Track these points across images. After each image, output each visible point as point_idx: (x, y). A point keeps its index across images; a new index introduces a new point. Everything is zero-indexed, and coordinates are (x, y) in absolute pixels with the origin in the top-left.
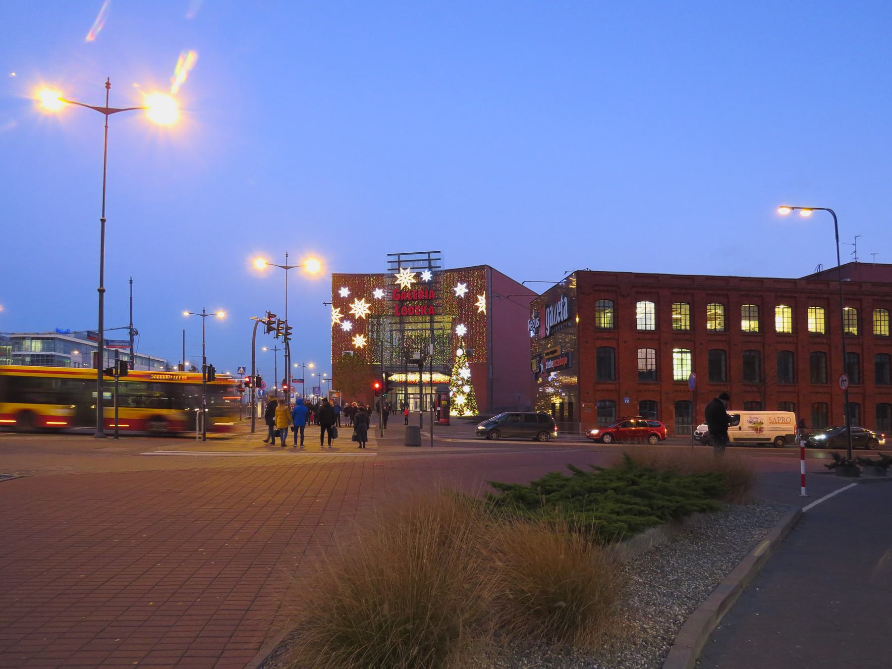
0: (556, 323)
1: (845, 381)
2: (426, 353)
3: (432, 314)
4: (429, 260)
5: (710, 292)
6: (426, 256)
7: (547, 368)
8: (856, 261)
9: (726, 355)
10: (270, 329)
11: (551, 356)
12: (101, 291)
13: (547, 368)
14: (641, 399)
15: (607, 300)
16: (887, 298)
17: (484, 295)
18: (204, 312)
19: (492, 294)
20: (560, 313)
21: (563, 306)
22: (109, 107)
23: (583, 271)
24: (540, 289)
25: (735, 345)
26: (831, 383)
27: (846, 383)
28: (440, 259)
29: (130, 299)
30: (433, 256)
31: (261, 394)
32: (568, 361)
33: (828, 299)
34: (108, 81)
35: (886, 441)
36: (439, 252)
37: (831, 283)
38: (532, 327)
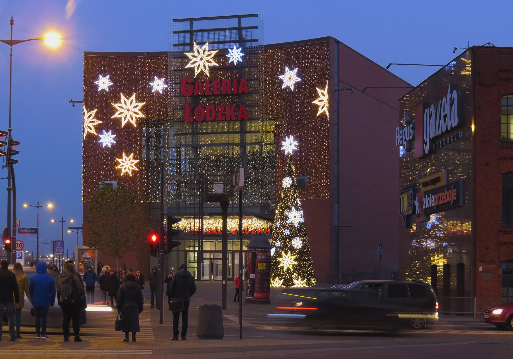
4: (240, 29)
6: (234, 23)
17: (327, 88)
30: (246, 22)
32: (458, 196)
36: (256, 15)
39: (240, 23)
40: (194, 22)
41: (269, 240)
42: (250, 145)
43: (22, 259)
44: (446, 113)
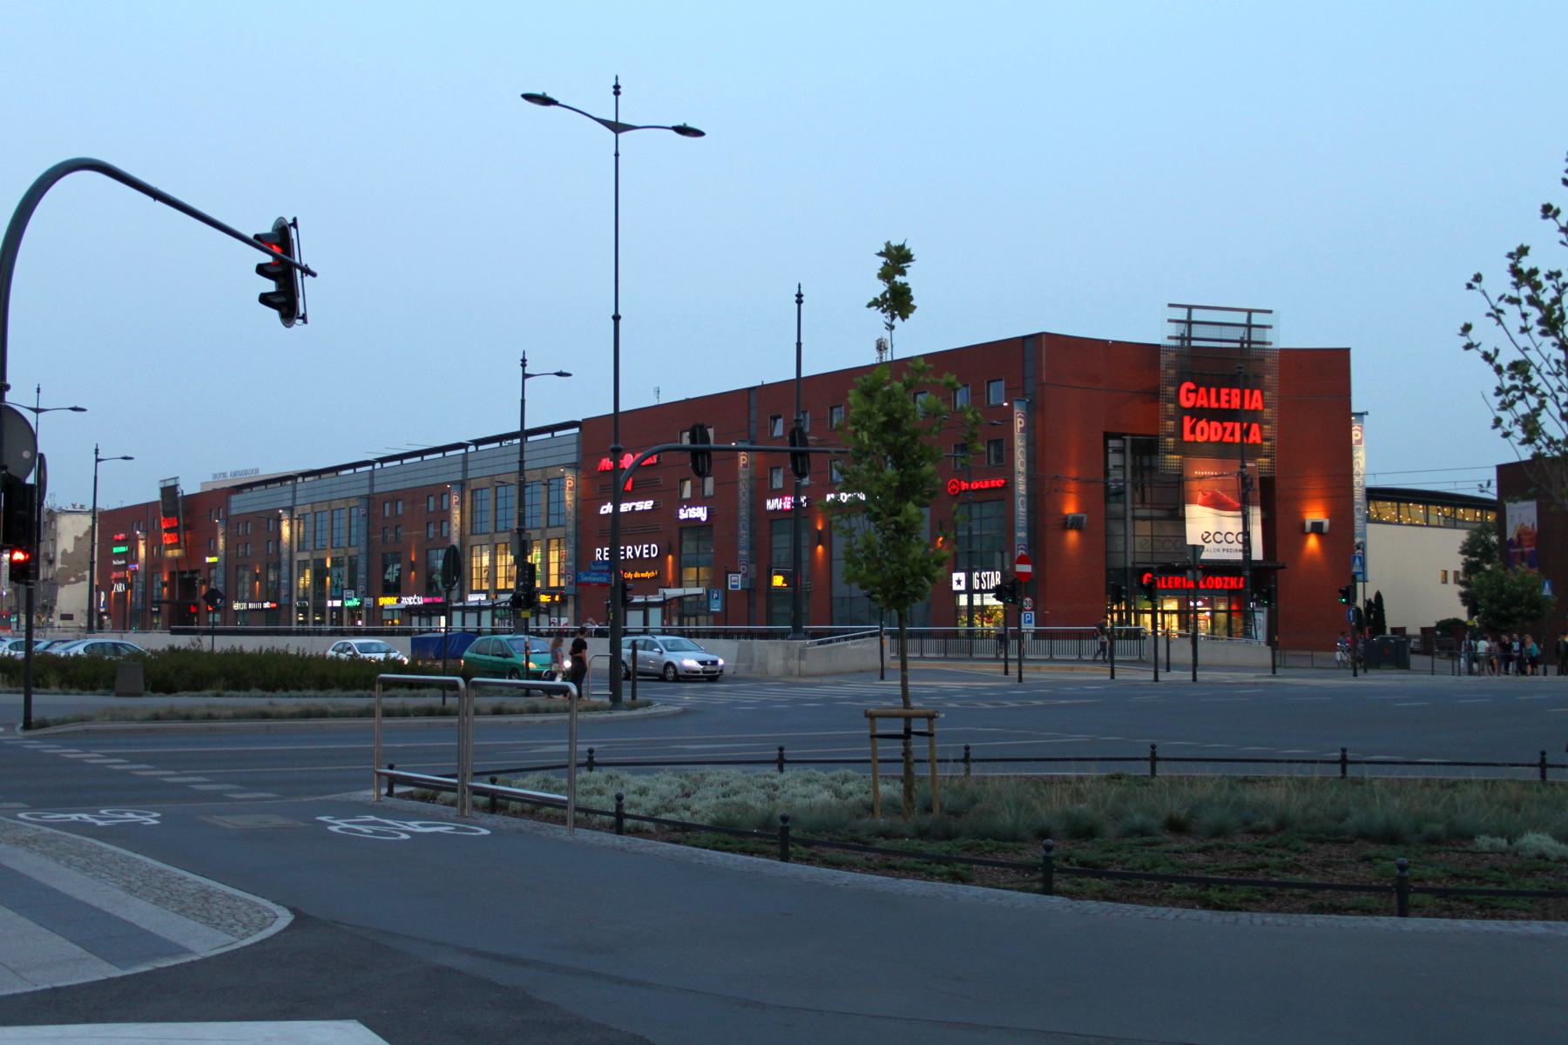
3: (1182, 348)
4: (1249, 326)
6: (1241, 318)
12: (616, 318)
22: (620, 121)
29: (795, 347)
30: (1257, 319)
34: (617, 83)
35: (111, 575)
36: (1270, 312)
39: (1189, 315)
40: (1194, 311)
41: (1477, 625)
42: (1444, 505)
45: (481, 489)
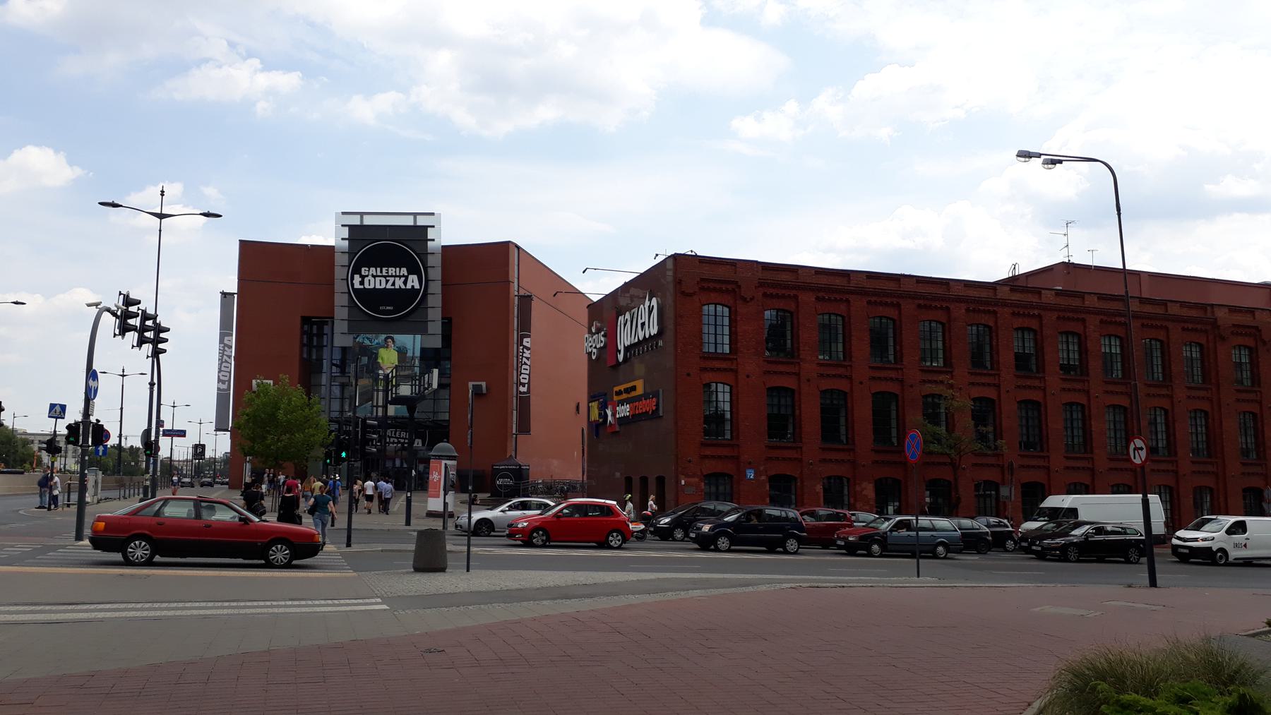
0: (636, 340)
1: (1142, 449)
2: (426, 386)
5: (873, 299)
7: (618, 416)
8: (1069, 261)
9: (897, 402)
10: (124, 329)
11: (625, 396)
13: (618, 416)
14: (773, 473)
15: (721, 304)
16: (1118, 319)
18: (123, 372)
19: (518, 292)
20: (643, 324)
21: (650, 312)
23: (684, 255)
24: (597, 287)
25: (911, 386)
26: (1048, 451)
27: (1143, 454)
28: (433, 227)
31: (101, 454)
32: (657, 405)
33: (1040, 316)
37: (1043, 292)
38: (591, 346)
43: (439, 497)
44: (643, 320)
45: (332, 359)
